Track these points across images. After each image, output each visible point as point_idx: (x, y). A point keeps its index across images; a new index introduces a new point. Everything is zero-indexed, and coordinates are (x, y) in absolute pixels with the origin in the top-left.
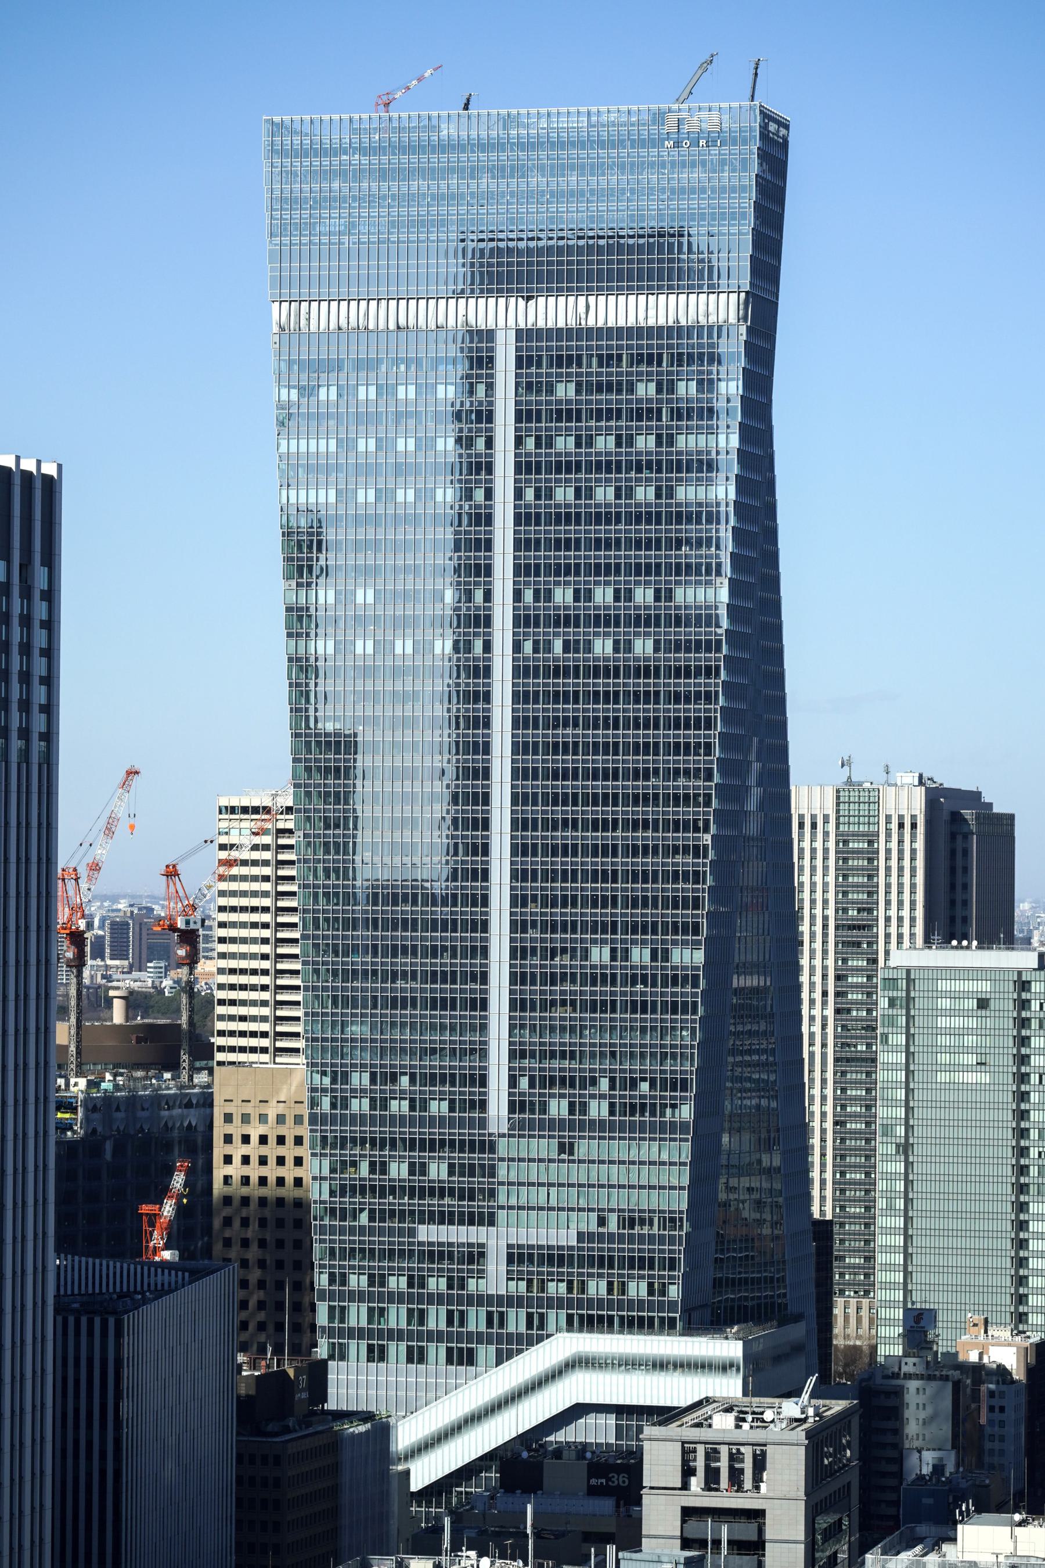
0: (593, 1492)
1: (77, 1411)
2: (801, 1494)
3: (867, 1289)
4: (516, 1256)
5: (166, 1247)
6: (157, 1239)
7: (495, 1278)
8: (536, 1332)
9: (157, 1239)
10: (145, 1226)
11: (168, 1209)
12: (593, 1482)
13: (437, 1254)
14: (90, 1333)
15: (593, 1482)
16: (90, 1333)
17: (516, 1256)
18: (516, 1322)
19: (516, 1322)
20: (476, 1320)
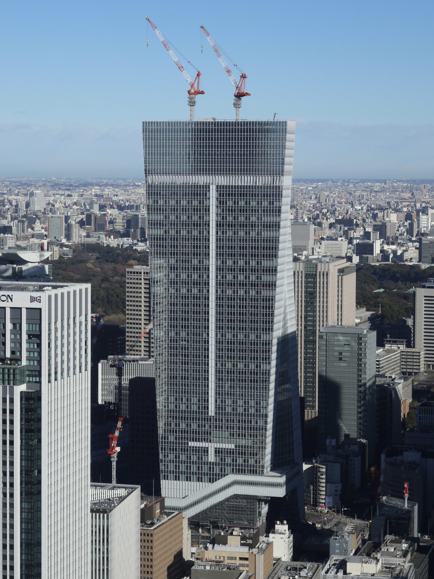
0: (242, 545)
1: (103, 539)
2: (195, 120)
3: (316, 504)
4: (217, 451)
5: (117, 446)
6: (114, 443)
7: (212, 458)
8: (223, 475)
9: (114, 443)
10: (111, 440)
11: (117, 434)
12: (242, 542)
13: (197, 450)
14: (103, 518)
15: (242, 542)
16: (103, 518)
17: (217, 451)
18: (217, 470)
19: (217, 470)
20: (205, 469)
